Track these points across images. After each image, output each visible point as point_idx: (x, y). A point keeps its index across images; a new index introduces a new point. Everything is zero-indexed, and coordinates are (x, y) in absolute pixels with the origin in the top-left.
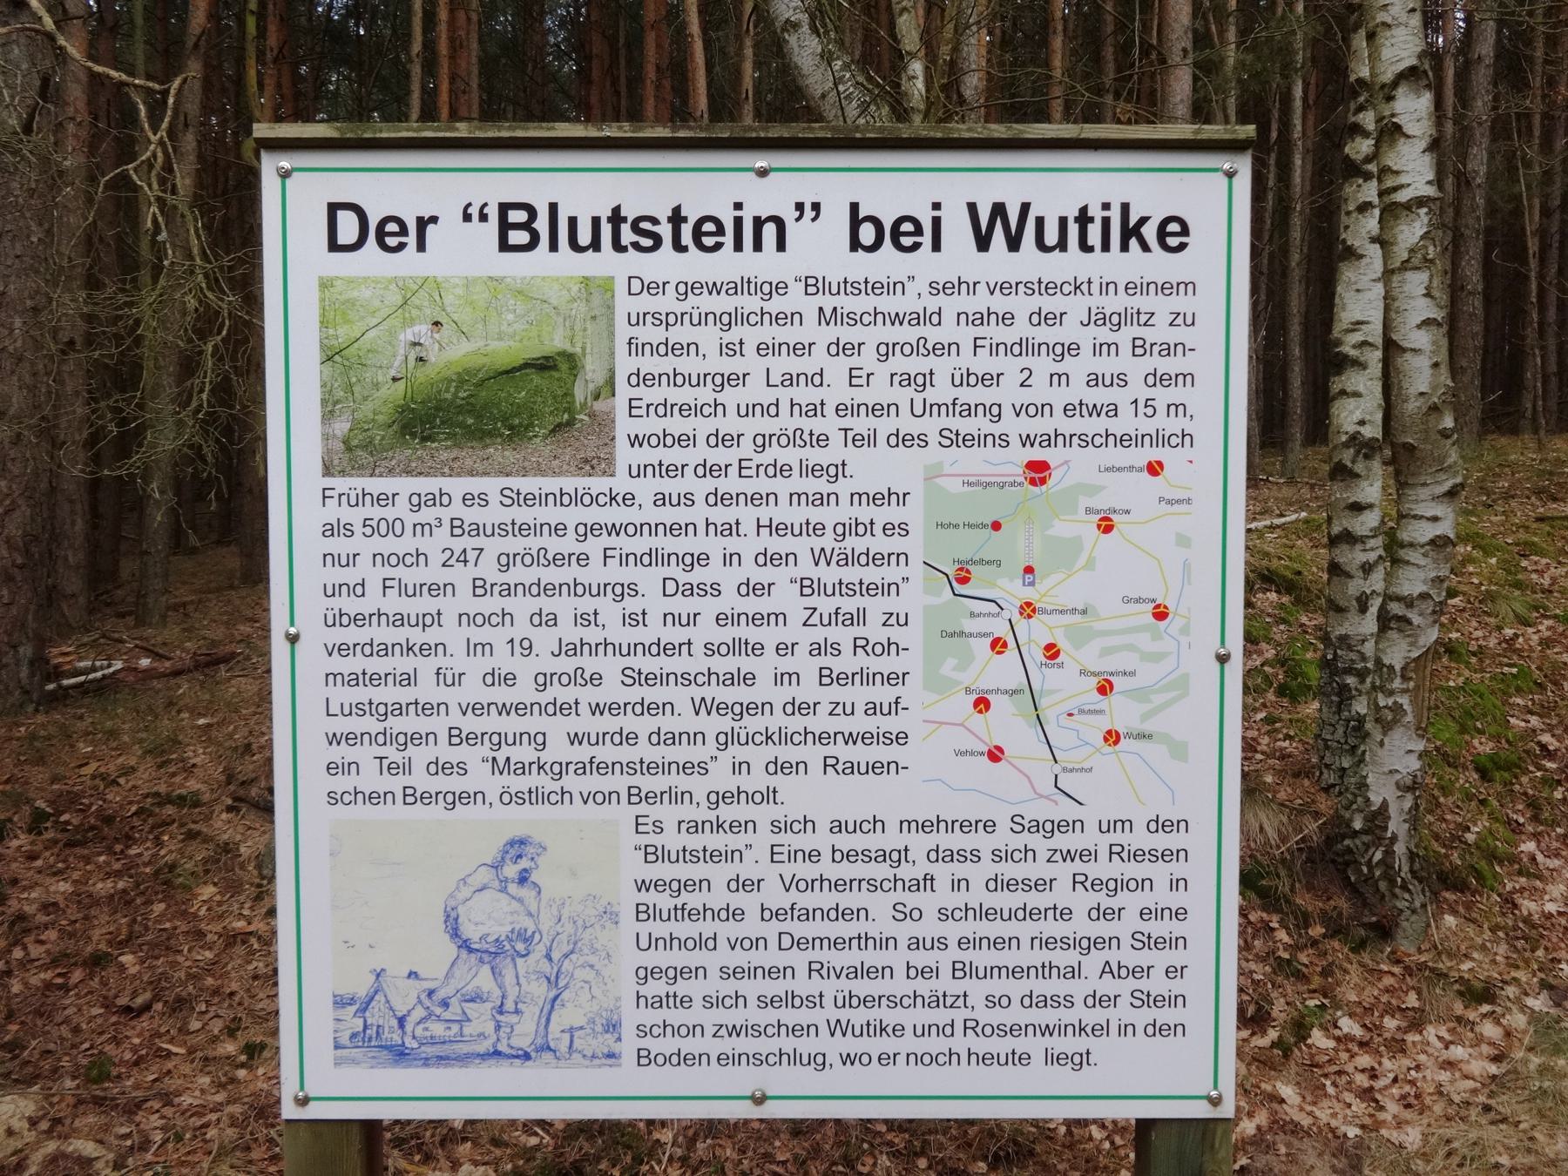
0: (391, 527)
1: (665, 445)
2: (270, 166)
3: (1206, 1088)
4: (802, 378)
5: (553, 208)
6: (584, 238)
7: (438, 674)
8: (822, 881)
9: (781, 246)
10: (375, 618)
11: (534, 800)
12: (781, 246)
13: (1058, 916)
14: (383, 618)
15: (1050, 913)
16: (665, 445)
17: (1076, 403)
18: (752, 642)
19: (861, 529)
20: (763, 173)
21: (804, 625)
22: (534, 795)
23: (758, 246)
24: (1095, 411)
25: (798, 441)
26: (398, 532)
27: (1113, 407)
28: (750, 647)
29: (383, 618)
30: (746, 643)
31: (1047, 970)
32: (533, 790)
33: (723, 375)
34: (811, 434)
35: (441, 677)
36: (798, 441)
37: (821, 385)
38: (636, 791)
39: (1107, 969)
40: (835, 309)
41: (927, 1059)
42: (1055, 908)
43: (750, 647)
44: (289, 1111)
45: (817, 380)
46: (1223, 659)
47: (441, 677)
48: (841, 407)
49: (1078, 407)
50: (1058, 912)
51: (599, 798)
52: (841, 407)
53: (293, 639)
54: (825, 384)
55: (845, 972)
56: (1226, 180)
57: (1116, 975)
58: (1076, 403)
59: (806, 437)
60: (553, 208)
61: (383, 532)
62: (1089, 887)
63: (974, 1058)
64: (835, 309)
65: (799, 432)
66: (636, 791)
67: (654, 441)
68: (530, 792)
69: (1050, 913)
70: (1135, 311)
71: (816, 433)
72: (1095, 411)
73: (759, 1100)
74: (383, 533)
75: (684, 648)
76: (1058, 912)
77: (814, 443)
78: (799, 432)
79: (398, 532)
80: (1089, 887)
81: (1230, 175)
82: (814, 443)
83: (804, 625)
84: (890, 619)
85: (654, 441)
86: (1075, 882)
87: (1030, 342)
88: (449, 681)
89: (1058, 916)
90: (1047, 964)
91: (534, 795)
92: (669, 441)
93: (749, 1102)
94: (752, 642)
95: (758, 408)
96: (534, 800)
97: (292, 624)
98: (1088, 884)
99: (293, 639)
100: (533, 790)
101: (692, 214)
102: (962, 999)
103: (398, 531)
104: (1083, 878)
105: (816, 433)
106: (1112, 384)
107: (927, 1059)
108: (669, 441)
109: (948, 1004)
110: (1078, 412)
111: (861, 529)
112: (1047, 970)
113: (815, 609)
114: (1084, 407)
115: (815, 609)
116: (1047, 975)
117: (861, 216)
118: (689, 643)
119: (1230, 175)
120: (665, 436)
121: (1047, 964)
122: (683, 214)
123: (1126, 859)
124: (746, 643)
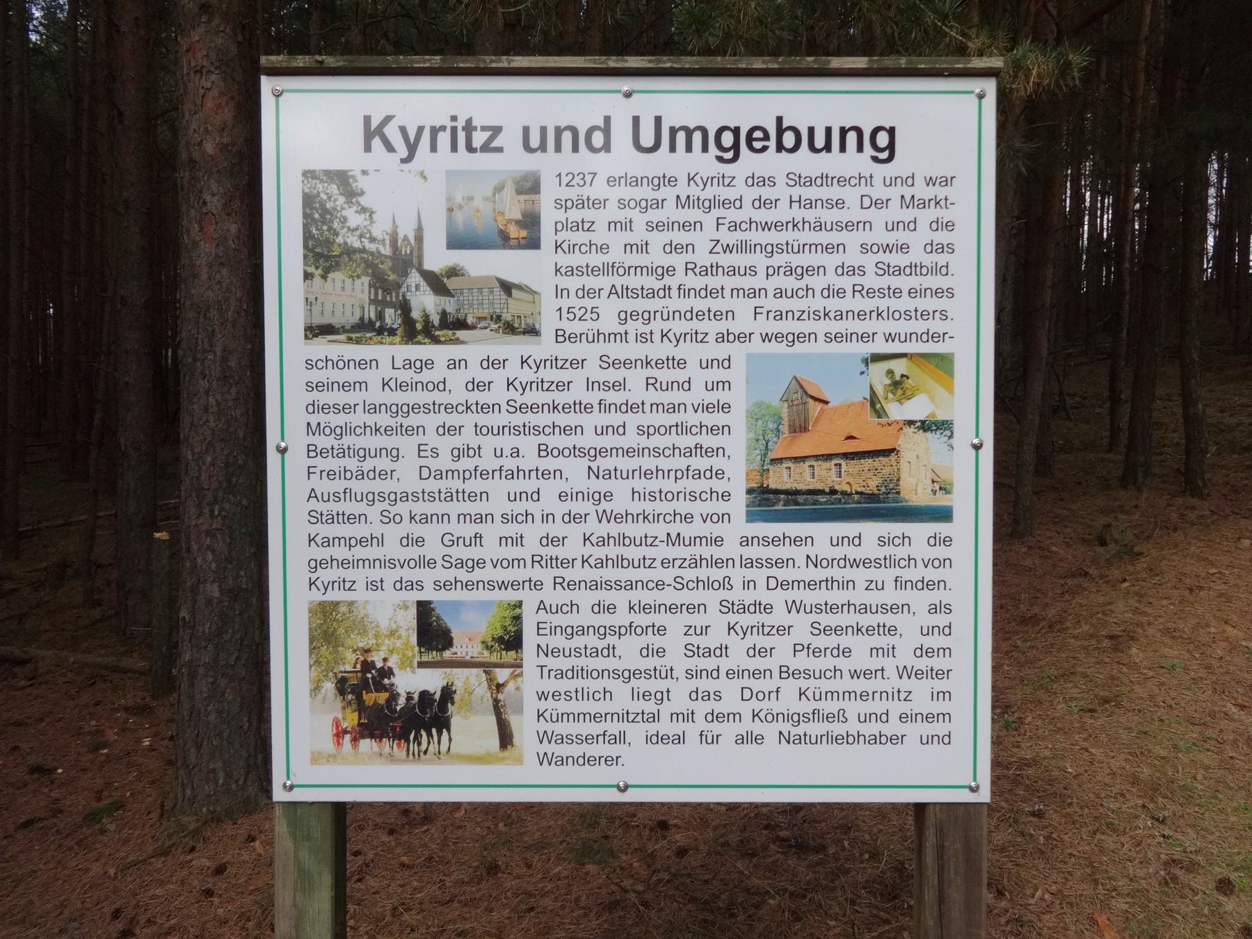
2: (267, 85)
5: (658, 120)
7: (701, 735)
8: (921, 267)
9: (526, 130)
10: (845, 608)
11: (888, 565)
12: (526, 130)
13: (656, 632)
14: (852, 608)
15: (527, 584)
18: (561, 558)
19: (471, 453)
20: (628, 95)
22: (888, 561)
29: (852, 608)
31: (714, 269)
32: (888, 557)
35: (704, 738)
38: (785, 669)
39: (542, 607)
40: (688, 197)
41: (430, 386)
42: (653, 626)
46: (977, 447)
47: (704, 738)
48: (611, 179)
50: (656, 629)
52: (611, 179)
53: (283, 451)
56: (977, 100)
57: (549, 611)
60: (658, 120)
62: (566, 587)
64: (688, 197)
66: (785, 669)
68: (885, 559)
69: (527, 584)
70: (696, 198)
73: (624, 789)
75: (879, 673)
76: (656, 629)
80: (566, 587)
84: (939, 226)
86: (555, 583)
88: (710, 740)
89: (532, 587)
90: (714, 265)
91: (888, 561)
93: (967, 790)
96: (888, 565)
98: (565, 585)
99: (283, 451)
100: (888, 557)
101: (427, 491)
102: (641, 715)
104: (561, 580)
106: (745, 274)
107: (430, 386)
109: (630, 720)
111: (471, 453)
112: (714, 269)
113: (718, 241)
115: (718, 241)
116: (714, 273)
118: (883, 670)
119: (981, 96)
121: (714, 265)
122: (474, 124)
123: (544, 565)
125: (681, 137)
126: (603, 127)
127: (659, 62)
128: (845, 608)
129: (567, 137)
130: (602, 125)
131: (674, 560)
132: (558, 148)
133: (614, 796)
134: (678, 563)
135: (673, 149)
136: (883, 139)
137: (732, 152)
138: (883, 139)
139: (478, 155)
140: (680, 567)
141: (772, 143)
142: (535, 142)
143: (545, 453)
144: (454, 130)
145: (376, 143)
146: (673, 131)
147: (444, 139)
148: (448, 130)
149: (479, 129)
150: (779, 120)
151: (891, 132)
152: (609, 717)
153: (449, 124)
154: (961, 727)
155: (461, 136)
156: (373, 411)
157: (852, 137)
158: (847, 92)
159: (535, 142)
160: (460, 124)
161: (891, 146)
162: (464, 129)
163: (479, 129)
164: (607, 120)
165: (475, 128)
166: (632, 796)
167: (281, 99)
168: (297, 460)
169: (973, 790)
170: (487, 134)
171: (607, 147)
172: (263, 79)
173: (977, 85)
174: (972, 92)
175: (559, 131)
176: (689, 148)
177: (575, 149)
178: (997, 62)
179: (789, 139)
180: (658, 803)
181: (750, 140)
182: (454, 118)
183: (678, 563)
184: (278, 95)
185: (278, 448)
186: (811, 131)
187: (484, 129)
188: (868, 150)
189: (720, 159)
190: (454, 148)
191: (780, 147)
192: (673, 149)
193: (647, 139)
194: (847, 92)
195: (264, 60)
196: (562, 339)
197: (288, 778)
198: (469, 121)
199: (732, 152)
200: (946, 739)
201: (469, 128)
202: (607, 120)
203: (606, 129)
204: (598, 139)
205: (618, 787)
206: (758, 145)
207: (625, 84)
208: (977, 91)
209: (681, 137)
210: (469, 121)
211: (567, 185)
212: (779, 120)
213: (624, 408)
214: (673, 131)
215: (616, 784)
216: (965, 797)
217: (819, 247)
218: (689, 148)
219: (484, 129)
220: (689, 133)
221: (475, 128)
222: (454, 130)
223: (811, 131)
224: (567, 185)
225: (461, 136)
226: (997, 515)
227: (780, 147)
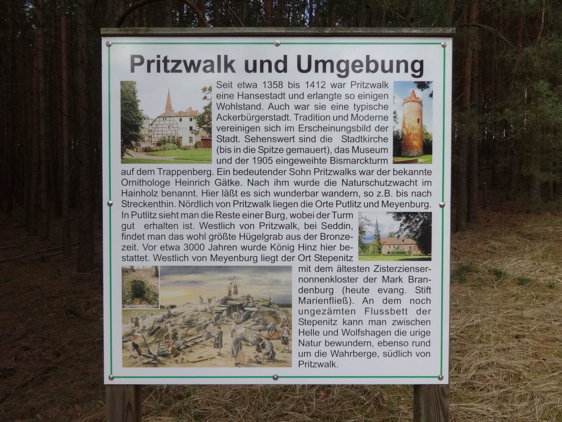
0: (199, 247)
1: (303, 218)
2: (104, 41)
3: (438, 374)
4: (253, 107)
5: (310, 57)
6: (376, 313)
9: (247, 62)
10: (152, 226)
12: (247, 62)
14: (155, 226)
16: (303, 218)
17: (242, 83)
18: (347, 267)
20: (277, 45)
21: (374, 271)
22: (174, 258)
23: (391, 62)
24: (171, 248)
25: (225, 238)
26: (202, 249)
27: (178, 247)
28: (346, 269)
29: (155, 226)
30: (345, 267)
33: (259, 116)
34: (230, 235)
36: (225, 238)
37: (260, 109)
43: (346, 269)
44: (107, 381)
45: (258, 107)
49: (165, 247)
51: (199, 259)
53: (110, 205)
54: (261, 109)
55: (388, 290)
58: (242, 83)
59: (228, 236)
60: (310, 57)
61: (191, 249)
63: (348, 290)
65: (225, 234)
67: (299, 216)
68: (173, 256)
71: (231, 235)
72: (171, 248)
74: (197, 249)
77: (231, 238)
78: (225, 234)
79: (202, 249)
81: (444, 46)
82: (231, 238)
83: (374, 271)
85: (299, 216)
87: (400, 352)
90: (161, 202)
91: (174, 258)
92: (304, 216)
94: (347, 267)
95: (288, 193)
97: (110, 200)
99: (110, 205)
103: (202, 248)
105: (231, 235)
108: (304, 216)
109: (365, 87)
110: (165, 248)
114: (168, 247)
117: (370, 60)
118: (294, 137)
119: (444, 46)
120: (303, 214)
121: (161, 202)
124: (345, 267)
125: (321, 65)
126: (283, 60)
127: (278, 30)
128: (152, 226)
129: (266, 65)
130: (283, 59)
131: (395, 268)
132: (262, 71)
133: (271, 382)
134: (397, 269)
135: (317, 71)
136: (417, 66)
137: (345, 72)
138: (417, 66)
139: (170, 74)
140: (398, 271)
141: (364, 68)
142: (251, 67)
143: (269, 216)
144: (159, 62)
145: (229, 69)
146: (317, 62)
147: (154, 66)
148: (156, 62)
149: (170, 61)
150: (368, 57)
151: (421, 63)
152: (366, 343)
153: (156, 59)
154: (434, 349)
155: (162, 65)
156: (180, 195)
157: (402, 65)
158: (133, 43)
159: (251, 67)
160: (162, 59)
161: (421, 70)
162: (163, 61)
163: (170, 61)
164: (285, 57)
165: (169, 61)
166: (280, 382)
167: (111, 47)
168: (117, 209)
169: (440, 378)
170: (175, 64)
171: (285, 70)
172: (103, 38)
173: (442, 41)
174: (440, 44)
175: (398, 63)
176: (324, 71)
177: (270, 71)
178: (450, 30)
179: (372, 66)
180: (379, 385)
181: (354, 66)
182: (158, 56)
183: (397, 269)
184: (109, 46)
185: (108, 203)
186: (383, 62)
187: (173, 61)
188: (336, 71)
189: (339, 76)
190: (159, 71)
191: (368, 70)
192: (317, 71)
193: (304, 66)
194: (133, 43)
195: (103, 31)
196: (333, 162)
197: (111, 374)
198: (166, 58)
199: (345, 72)
200: (427, 354)
201: (166, 61)
202: (285, 57)
203: (285, 62)
204: (281, 66)
205: (273, 377)
206: (357, 69)
207: (278, 40)
208: (443, 44)
209: (321, 65)
210: (166, 58)
211: (322, 87)
212: (368, 57)
213: (294, 194)
214: (317, 62)
215: (272, 376)
216: (436, 382)
217: (381, 117)
218: (324, 71)
219: (173, 61)
220: (325, 63)
221: (169, 61)
222: (159, 62)
223: (383, 62)
224: (322, 87)
225: (162, 65)
226: (101, 244)
227: (368, 70)
